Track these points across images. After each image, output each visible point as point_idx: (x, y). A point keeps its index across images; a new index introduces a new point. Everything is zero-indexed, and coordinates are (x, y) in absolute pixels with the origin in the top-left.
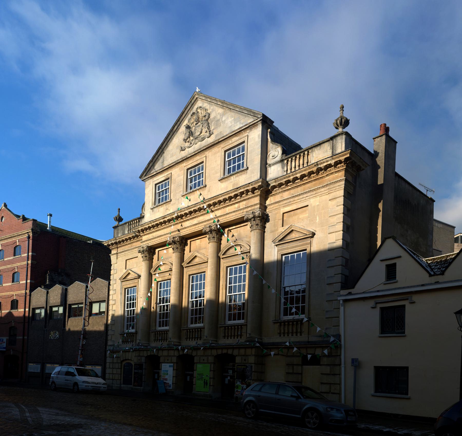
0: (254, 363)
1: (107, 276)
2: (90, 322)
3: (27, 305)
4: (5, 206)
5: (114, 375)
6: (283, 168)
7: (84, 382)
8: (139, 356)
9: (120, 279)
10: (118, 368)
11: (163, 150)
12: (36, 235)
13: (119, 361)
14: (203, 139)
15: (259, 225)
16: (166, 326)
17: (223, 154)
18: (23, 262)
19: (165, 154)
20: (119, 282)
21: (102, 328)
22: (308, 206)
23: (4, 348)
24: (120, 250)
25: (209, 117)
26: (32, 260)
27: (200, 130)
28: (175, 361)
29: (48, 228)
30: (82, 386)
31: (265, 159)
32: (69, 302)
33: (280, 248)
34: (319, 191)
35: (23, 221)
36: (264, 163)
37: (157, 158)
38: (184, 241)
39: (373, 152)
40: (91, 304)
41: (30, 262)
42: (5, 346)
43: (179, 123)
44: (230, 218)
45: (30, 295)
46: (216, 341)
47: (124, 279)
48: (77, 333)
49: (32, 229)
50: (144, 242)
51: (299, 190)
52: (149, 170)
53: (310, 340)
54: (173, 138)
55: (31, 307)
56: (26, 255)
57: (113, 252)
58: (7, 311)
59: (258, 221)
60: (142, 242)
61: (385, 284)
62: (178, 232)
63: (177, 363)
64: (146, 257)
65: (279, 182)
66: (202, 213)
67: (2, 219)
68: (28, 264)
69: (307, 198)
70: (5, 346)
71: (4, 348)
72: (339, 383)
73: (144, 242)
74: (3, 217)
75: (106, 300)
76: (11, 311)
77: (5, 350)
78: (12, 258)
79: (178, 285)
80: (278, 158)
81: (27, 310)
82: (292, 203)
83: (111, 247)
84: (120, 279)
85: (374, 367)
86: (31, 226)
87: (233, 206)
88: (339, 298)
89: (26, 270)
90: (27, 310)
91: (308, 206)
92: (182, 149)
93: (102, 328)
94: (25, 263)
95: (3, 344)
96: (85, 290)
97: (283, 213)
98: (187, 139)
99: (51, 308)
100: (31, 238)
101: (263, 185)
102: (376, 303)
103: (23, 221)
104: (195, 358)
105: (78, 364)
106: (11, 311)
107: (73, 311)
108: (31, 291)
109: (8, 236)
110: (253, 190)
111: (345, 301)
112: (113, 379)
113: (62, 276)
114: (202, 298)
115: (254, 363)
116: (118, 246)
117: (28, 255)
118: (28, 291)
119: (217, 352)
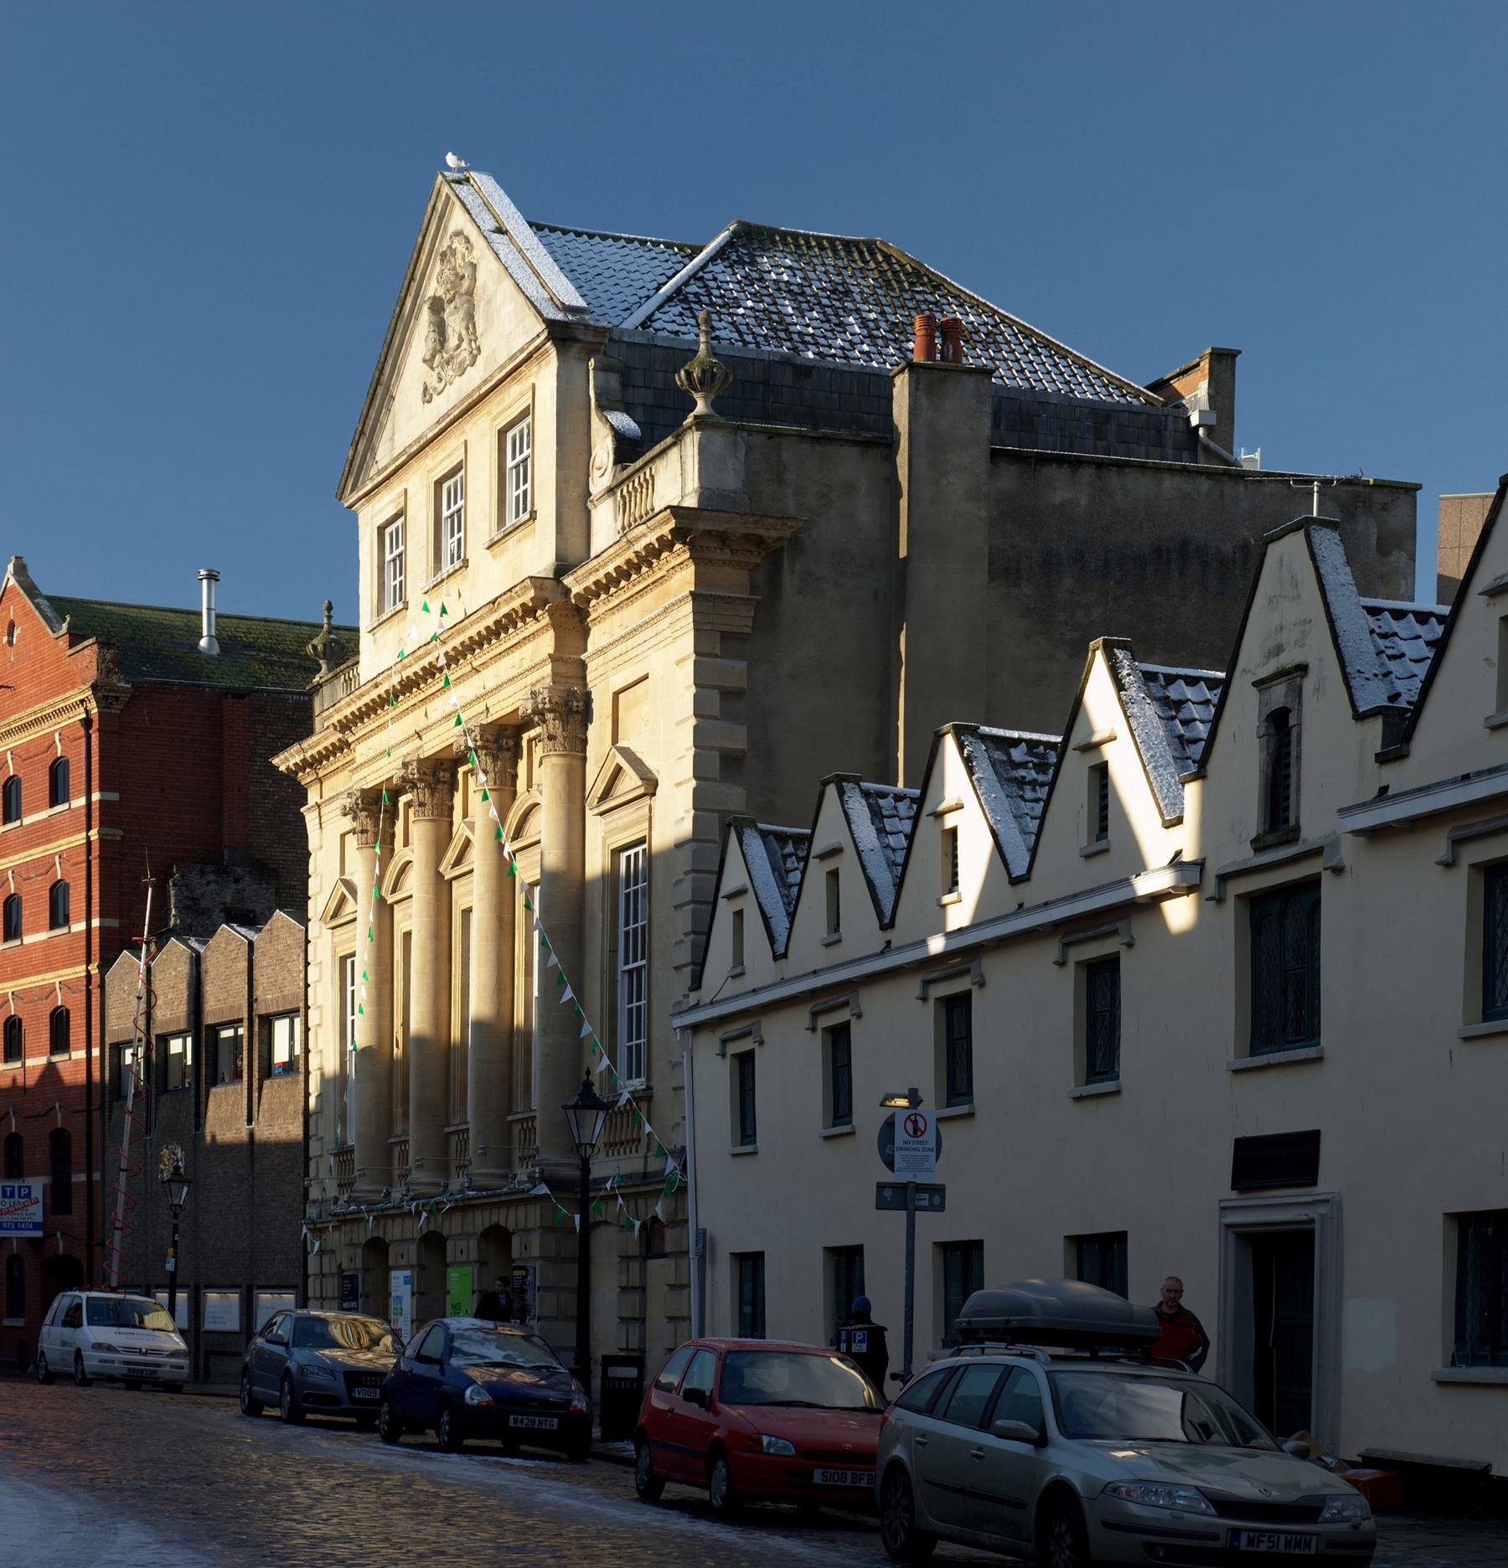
1: (298, 906)
3: (96, 1034)
4: (21, 570)
7: (98, 1346)
11: (388, 389)
12: (116, 709)
15: (560, 739)
18: (58, 840)
21: (295, 1131)
22: (646, 677)
23: (36, 1226)
26: (102, 824)
29: (203, 643)
30: (92, 1360)
31: (583, 477)
32: (209, 1019)
33: (613, 826)
35: (71, 646)
36: (574, 493)
37: (377, 420)
38: (444, 775)
40: (268, 1021)
41: (94, 834)
42: (39, 1218)
43: (414, 285)
44: (437, 741)
45: (102, 986)
47: (334, 917)
48: (231, 1148)
49: (94, 688)
52: (361, 468)
54: (410, 341)
55: (108, 1041)
57: (313, 797)
58: (42, 1061)
59: (553, 724)
61: (733, 977)
62: (417, 743)
64: (363, 832)
66: (401, 709)
67: (11, 634)
68: (89, 842)
70: (39, 1218)
71: (36, 1226)
74: (12, 626)
75: (302, 1005)
76: (55, 1059)
77: (39, 1234)
78: (43, 815)
79: (429, 956)
81: (96, 1052)
83: (305, 778)
86: (92, 674)
87: (516, 655)
89: (84, 873)
90: (96, 1052)
91: (646, 677)
93: (295, 1131)
94: (80, 838)
95: (31, 1209)
97: (616, 695)
98: (433, 357)
99: (164, 1039)
100: (96, 726)
101: (546, 594)
103: (71, 646)
105: (114, 1283)
106: (55, 1059)
107: (215, 1058)
108: (105, 966)
109: (26, 715)
110: (529, 612)
113: (237, 881)
114: (632, 966)
115: (542, 1258)
116: (321, 773)
117: (89, 803)
118: (94, 971)
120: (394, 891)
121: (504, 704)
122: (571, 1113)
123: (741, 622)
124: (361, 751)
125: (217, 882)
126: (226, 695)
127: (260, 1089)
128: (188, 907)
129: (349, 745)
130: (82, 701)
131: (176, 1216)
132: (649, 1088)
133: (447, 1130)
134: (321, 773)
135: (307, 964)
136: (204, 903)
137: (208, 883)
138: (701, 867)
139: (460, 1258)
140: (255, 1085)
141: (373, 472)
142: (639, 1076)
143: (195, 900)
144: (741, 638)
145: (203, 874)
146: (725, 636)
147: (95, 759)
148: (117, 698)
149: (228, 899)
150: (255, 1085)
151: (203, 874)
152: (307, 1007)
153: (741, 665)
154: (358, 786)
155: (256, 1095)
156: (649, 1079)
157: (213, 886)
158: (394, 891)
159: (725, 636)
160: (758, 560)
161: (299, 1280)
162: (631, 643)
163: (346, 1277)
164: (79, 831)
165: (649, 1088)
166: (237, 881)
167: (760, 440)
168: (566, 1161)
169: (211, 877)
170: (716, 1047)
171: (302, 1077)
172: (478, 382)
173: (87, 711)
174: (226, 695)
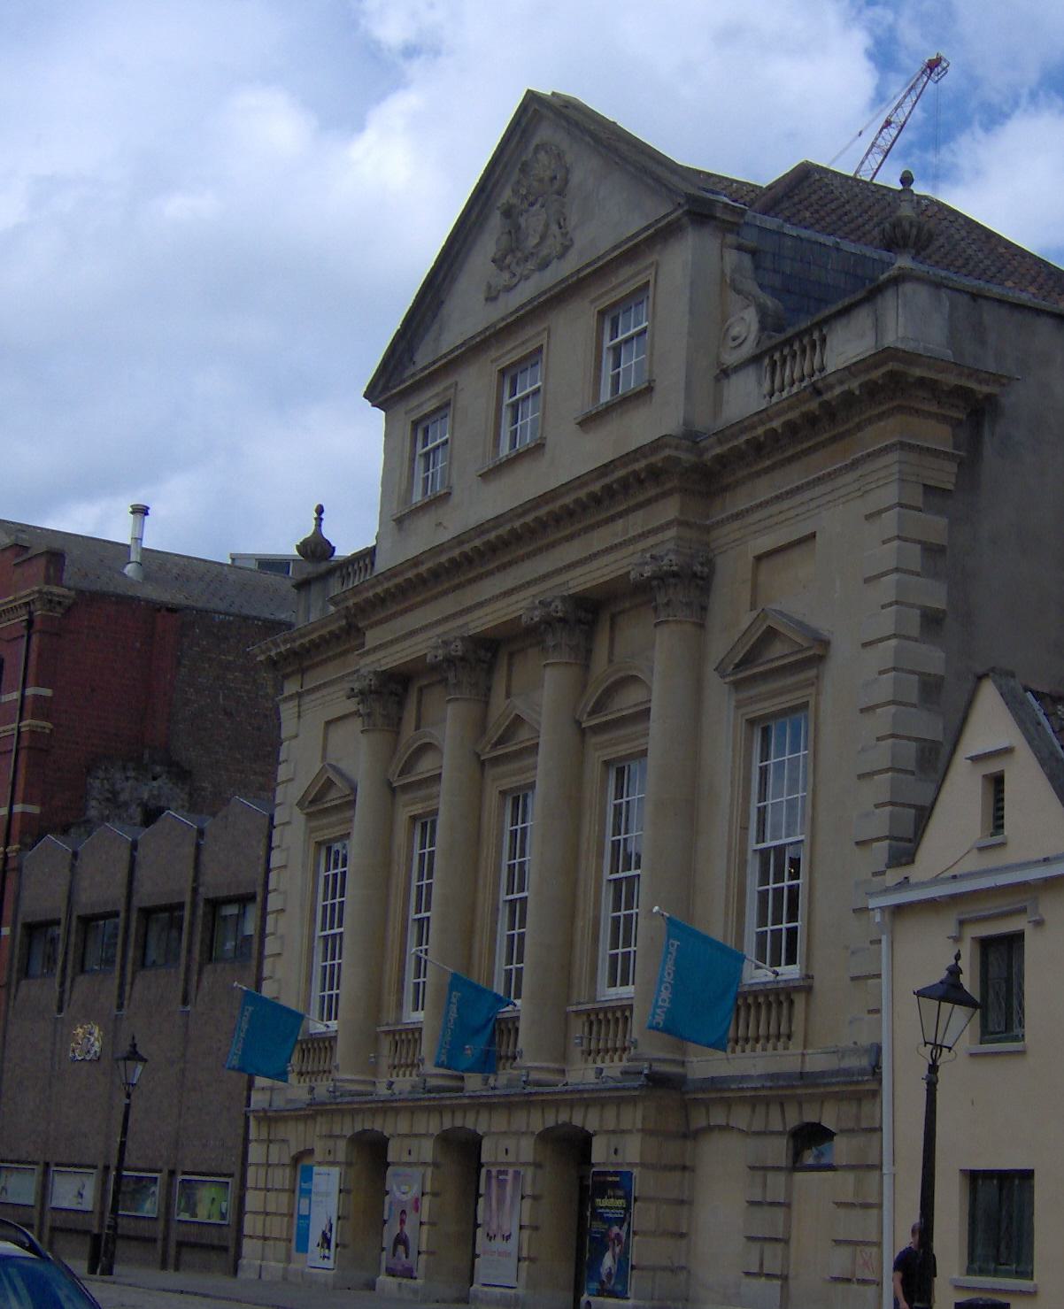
0: (642, 1165)
2: (205, 983)
5: (268, 1218)
6: (760, 384)
8: (331, 1136)
9: (300, 804)
10: (283, 1190)
13: (287, 1160)
14: (544, 265)
16: (625, 983)
17: (593, 322)
19: (446, 310)
20: (299, 817)
24: (312, 680)
25: (566, 181)
27: (540, 228)
28: (341, 1157)
29: (129, 570)
34: (840, 481)
39: (229, 562)
44: (599, 573)
46: (563, 1072)
50: (375, 649)
51: (793, 476)
53: (808, 1068)
56: (16, 695)
60: (362, 655)
61: (981, 849)
63: (349, 1164)
65: (731, 445)
69: (813, 504)
72: (874, 1238)
73: (375, 649)
80: (748, 350)
82: (775, 519)
84: (300, 804)
85: (963, 1171)
88: (873, 903)
92: (491, 299)
96: (192, 849)
102: (962, 923)
104: (486, 1144)
111: (898, 910)
112: (265, 1239)
115: (642, 1165)
116: (306, 663)
119: (571, 1118)
120: (402, 773)
121: (605, 571)
122: (121, 1064)
123: (945, 475)
124: (373, 637)
125: (137, 779)
126: (159, 610)
127: (200, 973)
128: (108, 800)
129: (358, 630)
130: (27, 604)
131: (128, 1096)
132: (808, 977)
133: (378, 1029)
134: (306, 663)
135: (270, 848)
136: (123, 797)
137: (127, 778)
138: (901, 732)
139: (406, 1158)
140: (195, 967)
141: (408, 373)
142: (791, 960)
143: (115, 794)
144: (945, 493)
145: (124, 768)
146: (929, 490)
147: (33, 656)
148: (60, 603)
149: (146, 796)
150: (195, 967)
151: (124, 768)
152: (266, 891)
153: (942, 522)
154: (371, 669)
155: (127, 988)
156: (808, 965)
157: (131, 782)
158: (402, 773)
159: (929, 490)
160: (962, 416)
161: (236, 1170)
162: (785, 504)
163: (797, 1155)
164: (13, 722)
165: (808, 977)
166: (154, 779)
167: (965, 299)
168: (669, 1056)
169: (131, 774)
170: (952, 929)
171: (254, 963)
172: (608, 246)
173: (31, 613)
174: (159, 610)
